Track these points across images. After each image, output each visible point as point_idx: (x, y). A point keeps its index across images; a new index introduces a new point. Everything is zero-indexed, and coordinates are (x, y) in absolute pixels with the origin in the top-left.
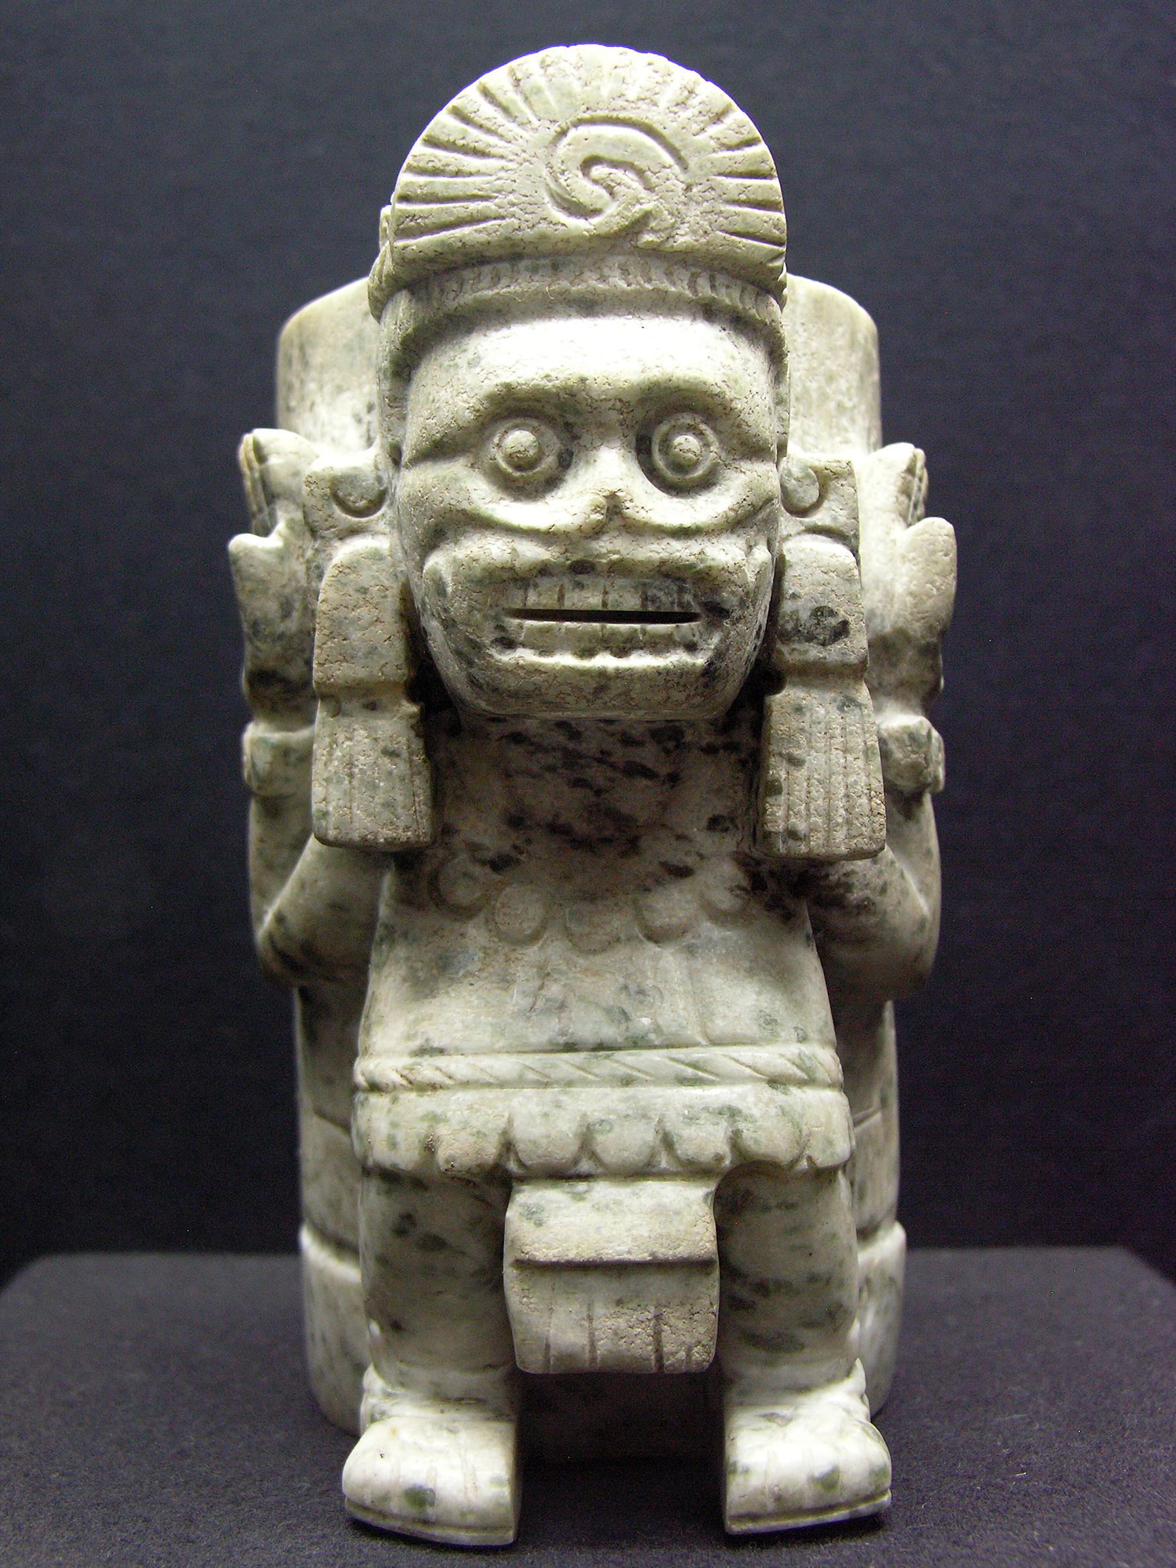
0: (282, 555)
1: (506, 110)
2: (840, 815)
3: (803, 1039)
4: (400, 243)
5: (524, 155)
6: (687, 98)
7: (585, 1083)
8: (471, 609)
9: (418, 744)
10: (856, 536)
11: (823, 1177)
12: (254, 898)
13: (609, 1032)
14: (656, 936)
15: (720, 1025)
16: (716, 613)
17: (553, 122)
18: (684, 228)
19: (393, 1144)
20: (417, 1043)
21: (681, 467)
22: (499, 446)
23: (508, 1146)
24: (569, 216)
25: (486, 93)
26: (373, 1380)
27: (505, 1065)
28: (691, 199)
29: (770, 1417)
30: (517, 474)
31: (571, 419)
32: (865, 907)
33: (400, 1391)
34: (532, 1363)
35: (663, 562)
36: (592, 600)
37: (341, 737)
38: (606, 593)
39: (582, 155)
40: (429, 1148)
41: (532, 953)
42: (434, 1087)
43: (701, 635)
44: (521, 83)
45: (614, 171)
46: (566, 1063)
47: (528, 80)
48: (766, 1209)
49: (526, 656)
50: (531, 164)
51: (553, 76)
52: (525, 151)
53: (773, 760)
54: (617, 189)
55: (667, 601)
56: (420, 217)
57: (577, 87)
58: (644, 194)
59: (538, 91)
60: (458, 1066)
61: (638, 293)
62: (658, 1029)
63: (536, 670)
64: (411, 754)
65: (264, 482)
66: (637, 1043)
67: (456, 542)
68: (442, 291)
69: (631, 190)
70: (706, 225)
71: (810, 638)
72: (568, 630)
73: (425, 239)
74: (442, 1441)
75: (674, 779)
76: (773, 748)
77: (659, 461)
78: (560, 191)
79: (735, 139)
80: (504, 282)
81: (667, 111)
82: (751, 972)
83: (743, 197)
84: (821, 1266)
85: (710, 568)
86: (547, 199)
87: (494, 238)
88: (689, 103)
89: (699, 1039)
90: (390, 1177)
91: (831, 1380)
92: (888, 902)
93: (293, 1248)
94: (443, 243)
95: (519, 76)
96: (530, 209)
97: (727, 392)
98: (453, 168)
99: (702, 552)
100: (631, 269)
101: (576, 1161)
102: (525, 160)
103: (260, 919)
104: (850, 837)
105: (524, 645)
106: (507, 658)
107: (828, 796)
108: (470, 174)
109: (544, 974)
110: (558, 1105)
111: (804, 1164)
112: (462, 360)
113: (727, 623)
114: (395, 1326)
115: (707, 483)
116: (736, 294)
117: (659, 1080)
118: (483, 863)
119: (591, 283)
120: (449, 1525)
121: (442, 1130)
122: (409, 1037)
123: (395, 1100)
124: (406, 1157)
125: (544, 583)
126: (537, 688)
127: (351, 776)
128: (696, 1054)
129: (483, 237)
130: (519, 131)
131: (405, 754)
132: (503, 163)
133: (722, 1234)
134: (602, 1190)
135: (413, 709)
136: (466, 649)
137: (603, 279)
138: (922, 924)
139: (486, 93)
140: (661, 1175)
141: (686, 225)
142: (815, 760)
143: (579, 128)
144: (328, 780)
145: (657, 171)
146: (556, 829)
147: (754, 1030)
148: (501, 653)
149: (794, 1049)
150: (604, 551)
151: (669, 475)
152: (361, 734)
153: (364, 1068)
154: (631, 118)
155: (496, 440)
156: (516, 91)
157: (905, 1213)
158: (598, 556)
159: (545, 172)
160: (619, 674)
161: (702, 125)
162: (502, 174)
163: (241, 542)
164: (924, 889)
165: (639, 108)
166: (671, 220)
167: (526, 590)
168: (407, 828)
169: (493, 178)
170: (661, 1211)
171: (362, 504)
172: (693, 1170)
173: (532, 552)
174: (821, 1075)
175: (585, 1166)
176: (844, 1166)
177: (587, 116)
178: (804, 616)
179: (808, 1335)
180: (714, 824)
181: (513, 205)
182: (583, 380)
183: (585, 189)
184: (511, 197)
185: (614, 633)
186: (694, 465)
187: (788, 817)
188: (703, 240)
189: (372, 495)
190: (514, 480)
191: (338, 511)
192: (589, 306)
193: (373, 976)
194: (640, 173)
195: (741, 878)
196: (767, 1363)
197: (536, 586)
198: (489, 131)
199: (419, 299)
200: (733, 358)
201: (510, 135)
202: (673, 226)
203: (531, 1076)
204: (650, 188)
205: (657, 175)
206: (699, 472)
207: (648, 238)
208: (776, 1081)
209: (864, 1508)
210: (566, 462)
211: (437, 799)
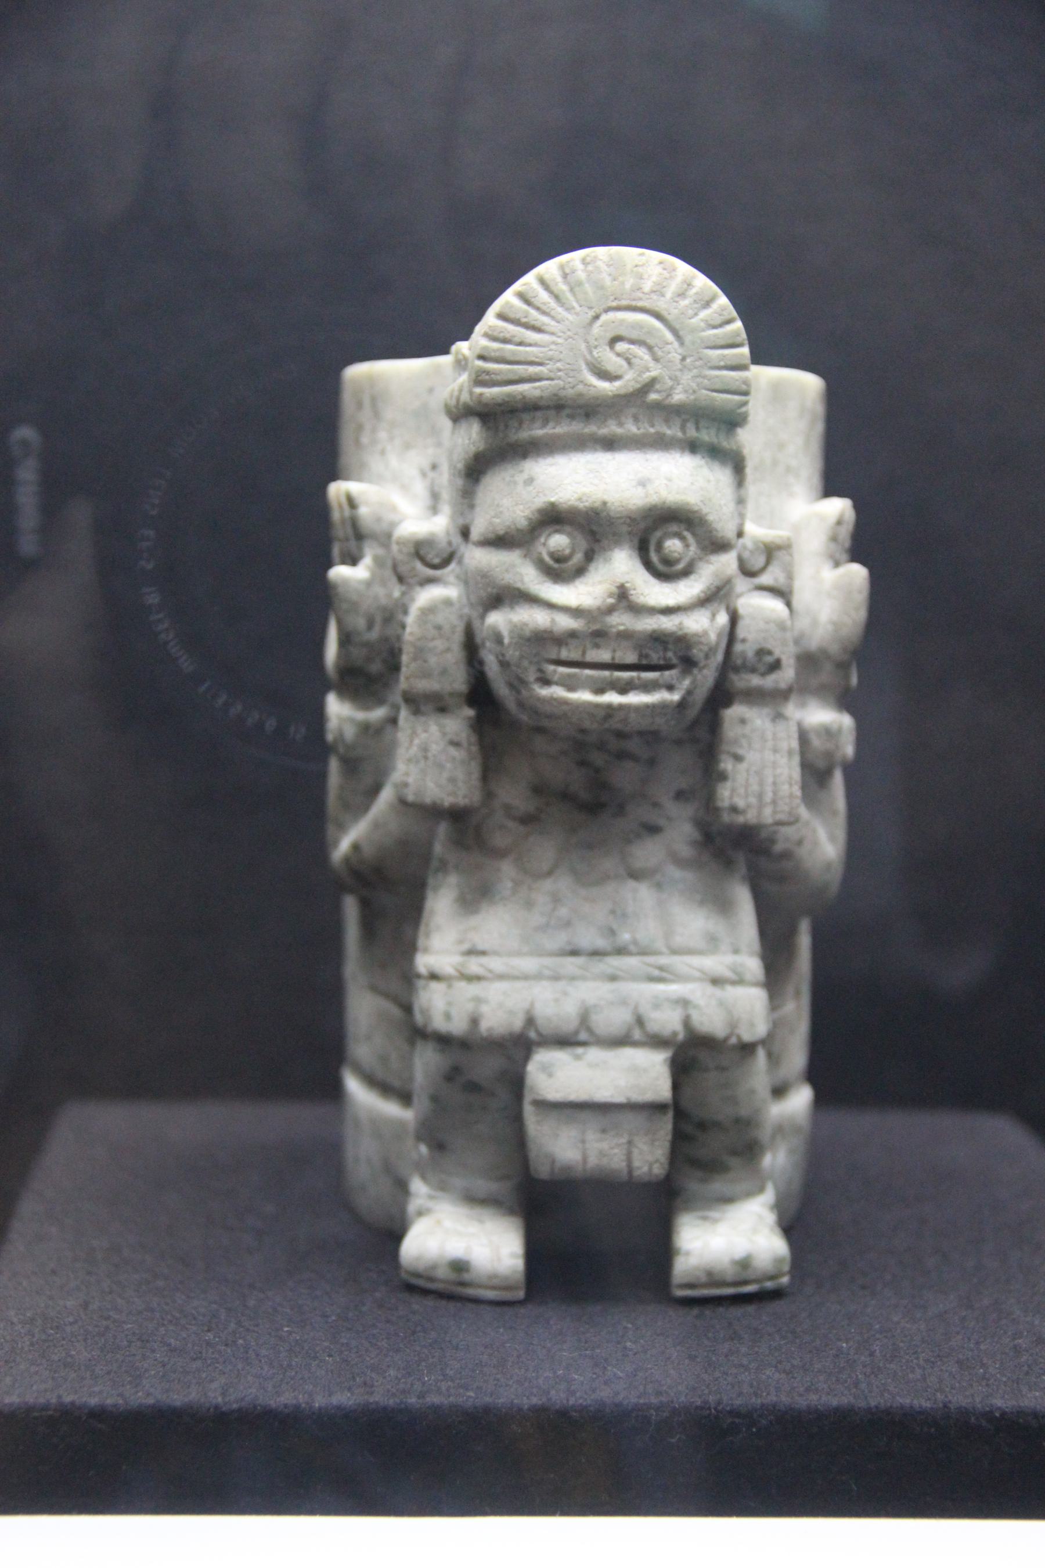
0: (369, 584)
1: (557, 297)
2: (769, 796)
3: (736, 951)
4: (478, 390)
5: (569, 333)
6: (686, 290)
7: (584, 978)
8: (522, 657)
9: (474, 739)
10: (791, 592)
11: (747, 1049)
12: (331, 830)
13: (601, 943)
14: (636, 875)
15: (678, 940)
16: (688, 663)
17: (591, 308)
18: (679, 389)
19: (448, 1016)
20: (466, 946)
21: (668, 562)
22: (544, 544)
23: (530, 1021)
24: (599, 379)
25: (542, 282)
26: (419, 1187)
27: (528, 964)
28: (685, 367)
29: (705, 1218)
30: (556, 566)
31: (594, 528)
32: (786, 855)
33: (439, 1194)
34: (542, 1171)
35: (654, 631)
36: (604, 655)
37: (419, 730)
38: (614, 651)
39: (609, 335)
40: (475, 1021)
41: (548, 885)
42: (478, 978)
43: (677, 679)
44: (569, 277)
45: (632, 347)
46: (571, 964)
47: (574, 274)
48: (706, 1070)
49: (559, 692)
50: (574, 340)
51: (592, 272)
52: (569, 330)
53: (723, 757)
54: (634, 360)
55: (655, 658)
56: (493, 373)
57: (608, 281)
58: (652, 364)
59: (580, 284)
60: (496, 964)
61: (645, 435)
62: (635, 942)
63: (565, 702)
64: (470, 744)
65: (354, 523)
66: (621, 951)
67: (512, 608)
68: (507, 426)
69: (644, 362)
70: (694, 385)
71: (753, 670)
72: (588, 677)
73: (496, 391)
74: (473, 1228)
75: (652, 762)
76: (724, 747)
77: (654, 558)
78: (594, 362)
79: (718, 320)
80: (551, 424)
81: (672, 301)
82: (702, 903)
83: (722, 364)
84: (744, 1112)
85: (686, 634)
86: (584, 367)
87: (546, 394)
88: (687, 293)
89: (664, 950)
90: (444, 1041)
91: (749, 1194)
92: (803, 852)
93: (335, 1092)
94: (509, 395)
95: (567, 271)
96: (572, 374)
97: (704, 509)
98: (517, 339)
99: (681, 624)
100: (641, 417)
101: (577, 1032)
102: (570, 337)
103: (336, 843)
104: (775, 812)
105: (557, 684)
106: (545, 692)
107: (761, 783)
108: (530, 345)
109: (556, 899)
110: (565, 994)
111: (733, 1040)
112: (520, 478)
113: (695, 671)
114: (439, 1147)
115: (687, 572)
116: (713, 432)
117: (634, 978)
118: (514, 819)
119: (611, 428)
120: (480, 1286)
121: (485, 1009)
122: (460, 942)
123: (450, 986)
124: (457, 1026)
125: (574, 642)
126: (565, 714)
127: (426, 758)
128: (663, 960)
129: (537, 393)
130: (565, 314)
131: (465, 744)
132: (554, 338)
133: (676, 1086)
134: (594, 1054)
135: (470, 712)
136: (516, 683)
137: (621, 424)
138: (828, 866)
139: (542, 282)
140: (635, 1044)
141: (681, 386)
142: (752, 757)
143: (609, 313)
144: (409, 760)
145: (662, 346)
146: (566, 796)
147: (699, 943)
148: (541, 687)
149: (729, 959)
150: (614, 623)
151: (661, 567)
152: (434, 728)
153: (423, 962)
154: (645, 307)
155: (542, 540)
156: (564, 282)
157: (813, 1075)
158: (612, 626)
159: (583, 346)
160: (621, 707)
161: (696, 311)
162: (553, 347)
163: (340, 572)
164: (832, 838)
165: (651, 299)
166: (670, 383)
167: (560, 648)
168: (465, 797)
169: (546, 349)
170: (635, 1069)
171: (437, 561)
172: (657, 1042)
173: (565, 623)
174: (748, 977)
175: (583, 1036)
176: (763, 1042)
177: (614, 304)
178: (750, 654)
179: (733, 1161)
180: (680, 795)
181: (560, 370)
182: (605, 503)
183: (611, 360)
184: (559, 365)
185: (619, 679)
186: (678, 561)
187: (731, 797)
188: (692, 397)
189: (445, 555)
190: (554, 569)
191: (419, 566)
192: (610, 444)
193: (430, 895)
194: (650, 348)
195: (697, 835)
196: (704, 1181)
197: (567, 644)
198: (544, 313)
199: (488, 429)
200: (709, 481)
201: (559, 317)
202: (672, 388)
203: (547, 972)
204: (656, 359)
205: (663, 349)
206: (680, 566)
207: (653, 396)
208: (716, 981)
209: (769, 1285)
210: (590, 557)
211: (485, 778)
